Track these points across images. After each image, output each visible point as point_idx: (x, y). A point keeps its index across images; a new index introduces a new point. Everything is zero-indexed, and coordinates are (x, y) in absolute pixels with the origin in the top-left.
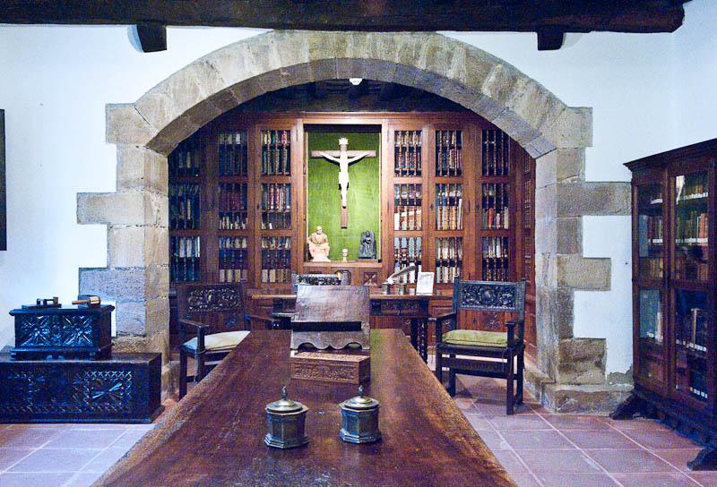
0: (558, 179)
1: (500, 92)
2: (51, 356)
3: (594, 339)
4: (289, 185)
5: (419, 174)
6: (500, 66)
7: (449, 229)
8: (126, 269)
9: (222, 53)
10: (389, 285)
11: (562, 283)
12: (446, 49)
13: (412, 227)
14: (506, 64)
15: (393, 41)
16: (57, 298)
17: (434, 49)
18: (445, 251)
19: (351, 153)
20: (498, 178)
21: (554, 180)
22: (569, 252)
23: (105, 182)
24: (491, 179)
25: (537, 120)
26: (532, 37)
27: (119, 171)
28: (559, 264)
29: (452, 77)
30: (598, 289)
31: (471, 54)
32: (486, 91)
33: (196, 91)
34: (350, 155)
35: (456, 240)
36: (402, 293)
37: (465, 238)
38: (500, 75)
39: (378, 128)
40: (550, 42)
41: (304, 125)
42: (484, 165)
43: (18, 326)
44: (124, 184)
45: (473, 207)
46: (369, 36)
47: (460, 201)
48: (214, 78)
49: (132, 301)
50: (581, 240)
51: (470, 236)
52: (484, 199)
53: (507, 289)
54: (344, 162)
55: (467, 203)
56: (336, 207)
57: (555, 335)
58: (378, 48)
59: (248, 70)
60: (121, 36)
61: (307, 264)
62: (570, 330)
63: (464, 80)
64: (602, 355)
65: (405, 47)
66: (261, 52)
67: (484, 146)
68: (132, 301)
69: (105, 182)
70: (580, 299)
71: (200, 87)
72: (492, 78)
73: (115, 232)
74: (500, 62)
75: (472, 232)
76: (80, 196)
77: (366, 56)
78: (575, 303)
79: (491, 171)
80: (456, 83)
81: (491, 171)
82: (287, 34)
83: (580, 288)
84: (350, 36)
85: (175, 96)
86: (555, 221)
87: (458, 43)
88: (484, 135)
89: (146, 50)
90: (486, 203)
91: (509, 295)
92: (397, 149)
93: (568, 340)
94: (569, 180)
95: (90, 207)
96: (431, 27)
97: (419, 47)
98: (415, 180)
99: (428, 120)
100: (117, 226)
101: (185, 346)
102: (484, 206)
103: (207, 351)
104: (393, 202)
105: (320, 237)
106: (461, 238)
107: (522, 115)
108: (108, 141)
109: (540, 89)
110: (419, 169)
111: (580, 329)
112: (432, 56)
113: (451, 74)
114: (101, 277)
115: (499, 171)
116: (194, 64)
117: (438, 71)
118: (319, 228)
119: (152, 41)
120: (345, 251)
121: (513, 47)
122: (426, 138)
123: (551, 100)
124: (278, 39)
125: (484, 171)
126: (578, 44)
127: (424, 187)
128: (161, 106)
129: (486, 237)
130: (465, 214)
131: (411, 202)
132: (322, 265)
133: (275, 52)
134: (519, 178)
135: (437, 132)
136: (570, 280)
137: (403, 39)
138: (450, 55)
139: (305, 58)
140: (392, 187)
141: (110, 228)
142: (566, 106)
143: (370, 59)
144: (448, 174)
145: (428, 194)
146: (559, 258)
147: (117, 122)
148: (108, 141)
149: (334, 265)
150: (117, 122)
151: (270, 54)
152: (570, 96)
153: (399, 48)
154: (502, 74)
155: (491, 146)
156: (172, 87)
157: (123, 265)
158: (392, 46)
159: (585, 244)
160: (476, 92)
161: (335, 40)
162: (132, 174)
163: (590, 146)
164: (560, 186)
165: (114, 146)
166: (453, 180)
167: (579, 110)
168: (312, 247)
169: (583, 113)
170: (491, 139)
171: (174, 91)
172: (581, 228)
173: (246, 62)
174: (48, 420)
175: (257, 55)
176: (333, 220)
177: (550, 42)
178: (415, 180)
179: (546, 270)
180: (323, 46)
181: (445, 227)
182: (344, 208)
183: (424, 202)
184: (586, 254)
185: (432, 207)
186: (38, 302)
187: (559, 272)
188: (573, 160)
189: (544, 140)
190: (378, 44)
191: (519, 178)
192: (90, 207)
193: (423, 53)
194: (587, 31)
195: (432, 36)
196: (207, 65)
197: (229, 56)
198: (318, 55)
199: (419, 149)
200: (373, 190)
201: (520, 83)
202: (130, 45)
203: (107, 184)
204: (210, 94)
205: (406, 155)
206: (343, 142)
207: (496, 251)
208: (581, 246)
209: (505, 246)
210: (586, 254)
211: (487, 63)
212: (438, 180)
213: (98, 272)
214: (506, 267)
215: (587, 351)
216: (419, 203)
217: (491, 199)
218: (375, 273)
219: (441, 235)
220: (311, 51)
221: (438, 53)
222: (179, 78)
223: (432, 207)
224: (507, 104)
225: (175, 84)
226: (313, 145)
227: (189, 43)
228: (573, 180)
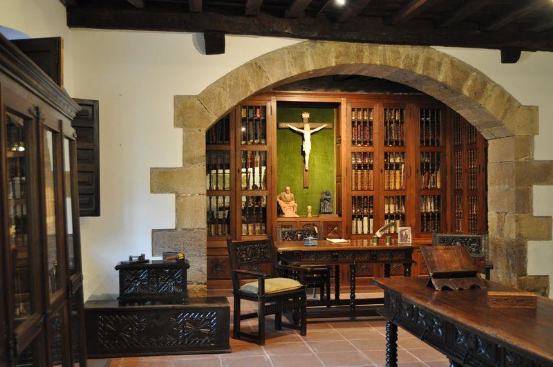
0: (516, 159)
1: (475, 93)
2: (149, 302)
3: (541, 276)
4: (92, 128)
5: (371, 144)
6: (475, 73)
7: (395, 189)
8: (190, 230)
9: (269, 57)
10: (378, 238)
11: (519, 235)
12: (437, 59)
13: (359, 188)
14: (479, 73)
15: (398, 52)
16: (144, 255)
17: (428, 60)
18: (392, 207)
19: (314, 125)
20: (433, 148)
21: (512, 159)
22: (524, 213)
23: (175, 160)
24: (428, 148)
25: (501, 115)
26: (496, 54)
27: (185, 151)
28: (516, 221)
29: (441, 81)
30: (543, 239)
31: (455, 64)
32: (466, 92)
33: (247, 86)
34: (313, 127)
35: (400, 199)
36: (375, 244)
37: (407, 197)
38: (475, 80)
39: (337, 105)
40: (510, 57)
41: (277, 102)
42: (422, 136)
43: (121, 277)
44: (188, 160)
45: (413, 172)
46: (381, 47)
47: (403, 165)
48: (262, 76)
49: (196, 255)
50: (532, 203)
51: (411, 195)
52: (422, 164)
53: (474, 240)
54: (307, 133)
55: (408, 168)
56: (299, 169)
57: (512, 274)
58: (387, 57)
59: (288, 71)
60: (186, 42)
61: (280, 219)
62: (525, 270)
63: (450, 83)
64: (546, 288)
65: (407, 56)
66: (298, 56)
67: (422, 122)
68: (196, 255)
69: (175, 160)
70: (531, 246)
71: (250, 83)
72: (470, 82)
73: (182, 200)
74: (475, 70)
75: (413, 192)
76: (151, 168)
77: (378, 63)
78: (528, 250)
79: (427, 142)
80: (444, 86)
81: (427, 142)
82: (318, 44)
83: (531, 239)
84: (366, 46)
85: (230, 90)
86: (514, 189)
87: (445, 55)
88: (422, 113)
89: (207, 53)
90: (425, 169)
91: (475, 244)
92: (353, 122)
93: (524, 278)
94: (523, 159)
95: (162, 180)
96: (425, 42)
97: (417, 57)
98: (368, 149)
99: (378, 98)
100: (183, 195)
101: (241, 291)
102: (422, 170)
103: (267, 294)
104: (350, 167)
105: (289, 196)
106: (404, 196)
107: (490, 110)
108: (176, 125)
109: (503, 93)
110: (371, 140)
111: (532, 269)
112: (426, 65)
113: (440, 78)
114: (170, 236)
115: (433, 141)
116: (246, 65)
117: (431, 76)
118: (288, 188)
119: (214, 46)
120: (309, 207)
121: (484, 60)
122: (376, 116)
123: (511, 99)
124: (312, 47)
125: (422, 142)
126: (530, 59)
127: (376, 154)
128: (219, 98)
129: (423, 195)
130: (407, 177)
131: (365, 166)
132: (292, 220)
133: (309, 57)
134: (448, 150)
135: (385, 110)
136: (524, 233)
137: (406, 51)
138: (440, 64)
139: (333, 62)
140: (350, 154)
141: (177, 197)
142: (521, 105)
143: (382, 65)
144: (395, 144)
145: (378, 161)
146: (516, 216)
147: (184, 109)
148: (176, 125)
149: (302, 220)
150: (184, 109)
151: (305, 59)
152: (523, 97)
153: (403, 57)
154: (476, 79)
155: (427, 122)
156: (228, 82)
157: (188, 226)
158: (397, 55)
159: (535, 206)
160: (457, 92)
161: (355, 49)
162: (196, 153)
163: (538, 134)
164: (518, 163)
165: (180, 131)
166: (397, 149)
167: (529, 108)
168: (282, 204)
169: (532, 110)
170: (427, 117)
171: (230, 86)
172: (532, 194)
173: (287, 64)
174: (142, 354)
175: (295, 59)
176: (297, 181)
177: (510, 57)
178: (368, 149)
179: (500, 221)
180: (346, 55)
181: (392, 187)
182: (307, 171)
183: (375, 167)
184: (535, 214)
185: (382, 171)
186: (131, 258)
187: (517, 227)
188: (526, 144)
189: (505, 128)
190: (387, 54)
191: (448, 150)
192: (162, 180)
193: (421, 61)
194: (535, 50)
195: (426, 50)
196: (256, 66)
197: (273, 59)
198: (342, 60)
199: (371, 123)
200: (330, 156)
201: (489, 87)
202: (194, 48)
203: (177, 162)
204: (258, 89)
205: (362, 128)
206: (306, 115)
207: (430, 207)
208: (532, 208)
209: (437, 205)
210: (535, 214)
211: (464, 71)
212: (387, 149)
213: (168, 233)
214: (439, 219)
215: (536, 286)
216: (371, 166)
217: (427, 164)
218: (337, 226)
219: (389, 194)
220: (337, 57)
221: (431, 62)
222: (234, 76)
223: (382, 171)
224: (480, 102)
225: (231, 81)
226: (280, 118)
227: (244, 49)
228: (526, 159)
